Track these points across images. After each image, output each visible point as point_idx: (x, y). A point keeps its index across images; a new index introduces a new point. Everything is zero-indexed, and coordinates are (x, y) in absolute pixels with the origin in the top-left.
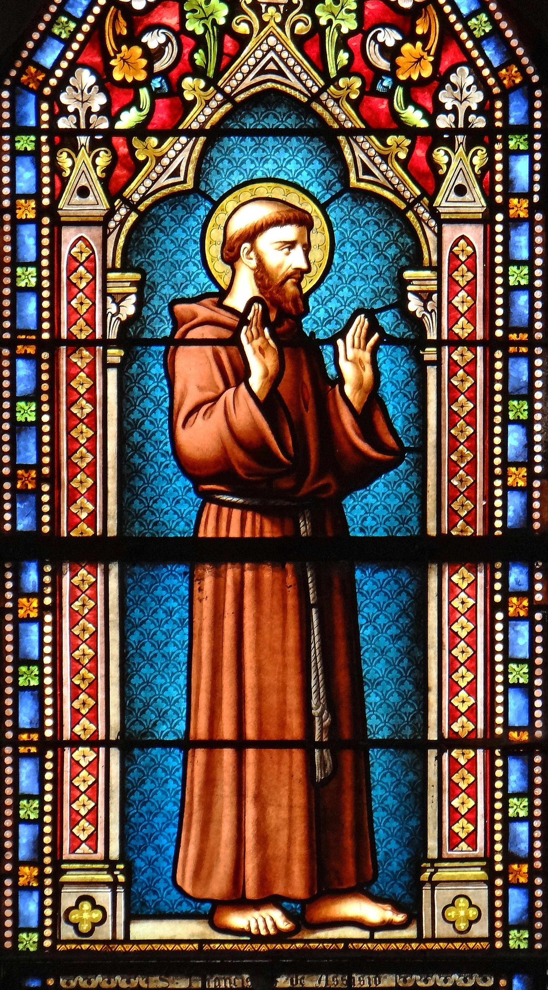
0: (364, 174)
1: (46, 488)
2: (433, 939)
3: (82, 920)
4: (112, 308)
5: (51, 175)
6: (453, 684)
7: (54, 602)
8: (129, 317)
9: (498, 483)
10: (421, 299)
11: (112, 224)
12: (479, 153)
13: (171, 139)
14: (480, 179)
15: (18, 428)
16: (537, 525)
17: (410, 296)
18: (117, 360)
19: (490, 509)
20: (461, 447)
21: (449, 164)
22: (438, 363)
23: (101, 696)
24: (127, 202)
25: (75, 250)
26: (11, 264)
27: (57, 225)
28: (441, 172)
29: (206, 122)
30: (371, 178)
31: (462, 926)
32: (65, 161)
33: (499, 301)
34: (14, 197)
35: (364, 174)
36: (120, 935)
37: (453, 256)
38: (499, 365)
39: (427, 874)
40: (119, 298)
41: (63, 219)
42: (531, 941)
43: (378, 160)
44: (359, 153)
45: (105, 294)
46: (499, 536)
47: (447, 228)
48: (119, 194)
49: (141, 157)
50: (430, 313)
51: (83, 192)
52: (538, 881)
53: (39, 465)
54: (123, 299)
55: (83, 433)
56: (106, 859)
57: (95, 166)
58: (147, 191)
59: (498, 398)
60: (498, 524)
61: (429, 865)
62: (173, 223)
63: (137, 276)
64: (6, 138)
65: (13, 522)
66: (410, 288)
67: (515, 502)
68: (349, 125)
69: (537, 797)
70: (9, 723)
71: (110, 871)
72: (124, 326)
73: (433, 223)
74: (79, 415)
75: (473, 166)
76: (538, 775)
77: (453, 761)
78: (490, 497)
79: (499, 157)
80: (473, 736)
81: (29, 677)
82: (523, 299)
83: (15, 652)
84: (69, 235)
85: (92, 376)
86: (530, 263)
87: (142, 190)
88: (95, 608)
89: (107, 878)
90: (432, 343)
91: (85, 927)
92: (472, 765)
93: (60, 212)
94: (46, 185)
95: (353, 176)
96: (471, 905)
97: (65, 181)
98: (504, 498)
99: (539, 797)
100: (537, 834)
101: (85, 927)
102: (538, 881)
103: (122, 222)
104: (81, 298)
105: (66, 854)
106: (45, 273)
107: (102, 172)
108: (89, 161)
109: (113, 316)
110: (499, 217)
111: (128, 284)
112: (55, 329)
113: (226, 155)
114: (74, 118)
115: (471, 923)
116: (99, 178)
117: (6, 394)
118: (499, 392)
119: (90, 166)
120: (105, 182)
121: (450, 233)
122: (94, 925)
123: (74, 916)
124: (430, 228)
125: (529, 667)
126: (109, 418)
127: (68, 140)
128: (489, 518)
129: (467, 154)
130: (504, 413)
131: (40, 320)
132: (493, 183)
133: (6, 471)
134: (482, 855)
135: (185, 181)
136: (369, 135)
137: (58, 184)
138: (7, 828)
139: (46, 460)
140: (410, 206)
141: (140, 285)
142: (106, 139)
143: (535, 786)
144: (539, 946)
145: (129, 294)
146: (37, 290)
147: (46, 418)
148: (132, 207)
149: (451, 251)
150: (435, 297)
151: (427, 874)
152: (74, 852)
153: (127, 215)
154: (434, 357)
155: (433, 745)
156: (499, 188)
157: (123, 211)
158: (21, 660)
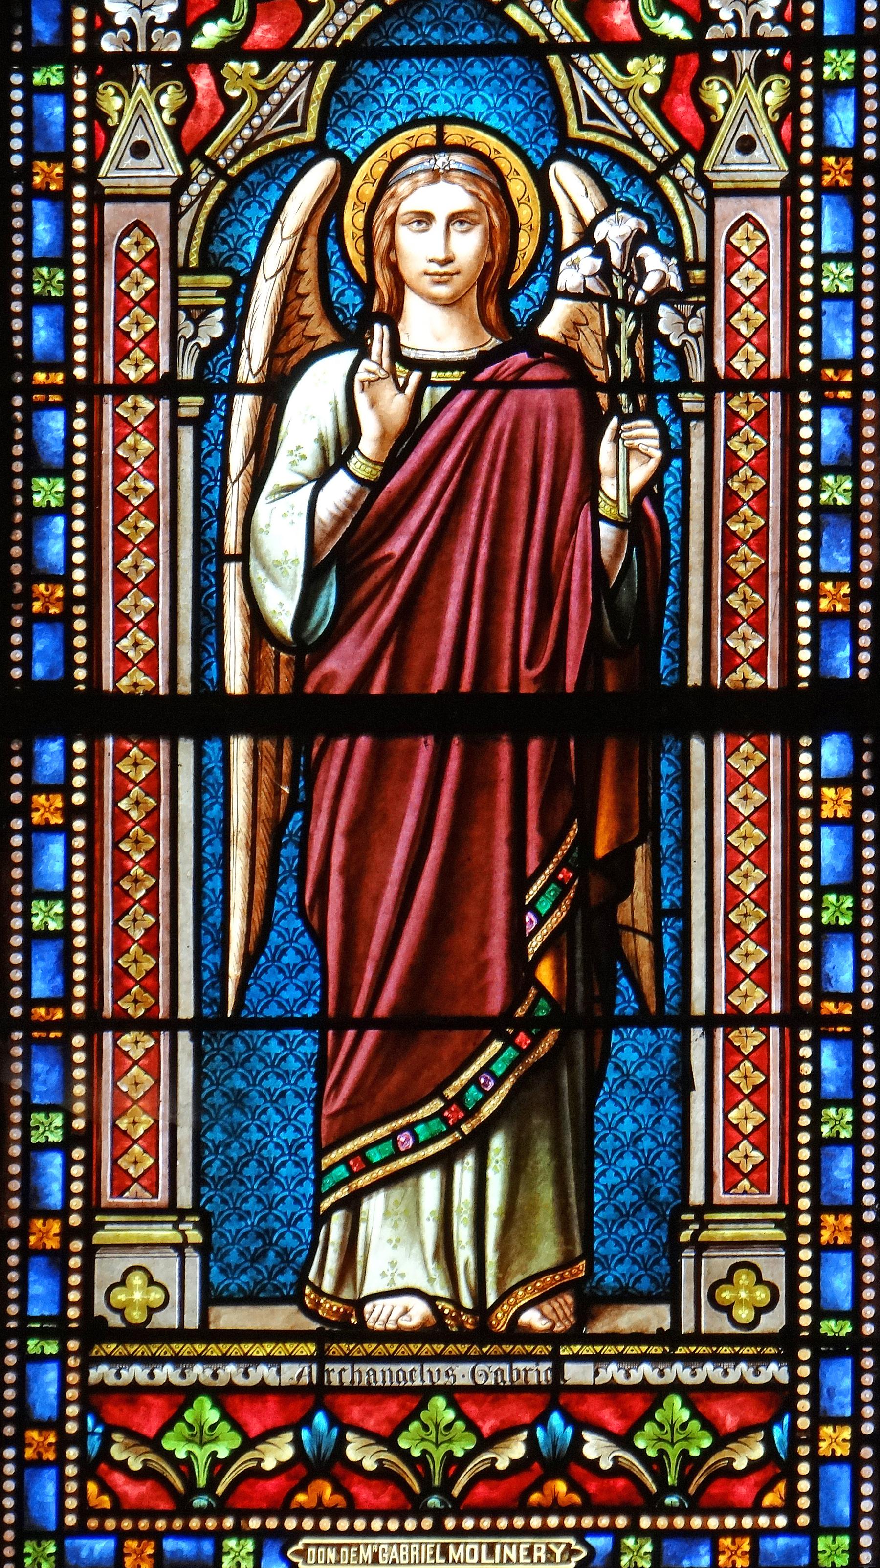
0: (590, 117)
1: (79, 825)
3: (130, 1302)
4: (187, 329)
8: (215, 20)
9: (803, 606)
11: (185, 200)
13: (281, 64)
22: (708, 417)
23: (164, 1109)
24: (209, 163)
25: (126, 241)
27: (97, 199)
29: (339, 34)
30: (602, 124)
31: (744, 1315)
32: (111, 101)
35: (590, 117)
36: (193, 1322)
38: (806, 313)
40: (196, 314)
43: (613, 96)
44: (583, 87)
45: (175, 307)
48: (198, 151)
51: (747, 145)
54: (203, 317)
56: (171, 1207)
57: (160, 109)
60: (804, 671)
61: (691, 1217)
62: (281, 976)
63: (224, 281)
65: (26, 664)
68: (565, 39)
70: (16, 993)
72: (205, 355)
73: (700, 193)
75: (765, 107)
76: (870, 80)
77: (731, 1049)
80: (763, 374)
82: (845, 1161)
83: (27, 880)
89: (173, 1236)
92: (761, 420)
93: (103, 182)
94: (78, 216)
96: (760, 1281)
97: (110, 132)
98: (815, 838)
99: (871, 1108)
102: (868, 816)
103: (204, 194)
105: (107, 1199)
107: (172, 115)
113: (368, 88)
114: (126, 34)
115: (151, 1282)
116: (166, 126)
117: (18, 255)
118: (807, 1095)
120: (174, 132)
121: (728, 210)
124: (695, 200)
126: (181, 528)
127: (119, 69)
128: (788, 662)
132: (797, 133)
135: (303, 129)
136: (596, 52)
137: (101, 135)
138: (8, 1369)
142: (179, 67)
143: (863, 878)
145: (213, 308)
147: (79, 925)
153: (211, 185)
154: (701, 408)
157: (204, 178)
158: (36, 466)
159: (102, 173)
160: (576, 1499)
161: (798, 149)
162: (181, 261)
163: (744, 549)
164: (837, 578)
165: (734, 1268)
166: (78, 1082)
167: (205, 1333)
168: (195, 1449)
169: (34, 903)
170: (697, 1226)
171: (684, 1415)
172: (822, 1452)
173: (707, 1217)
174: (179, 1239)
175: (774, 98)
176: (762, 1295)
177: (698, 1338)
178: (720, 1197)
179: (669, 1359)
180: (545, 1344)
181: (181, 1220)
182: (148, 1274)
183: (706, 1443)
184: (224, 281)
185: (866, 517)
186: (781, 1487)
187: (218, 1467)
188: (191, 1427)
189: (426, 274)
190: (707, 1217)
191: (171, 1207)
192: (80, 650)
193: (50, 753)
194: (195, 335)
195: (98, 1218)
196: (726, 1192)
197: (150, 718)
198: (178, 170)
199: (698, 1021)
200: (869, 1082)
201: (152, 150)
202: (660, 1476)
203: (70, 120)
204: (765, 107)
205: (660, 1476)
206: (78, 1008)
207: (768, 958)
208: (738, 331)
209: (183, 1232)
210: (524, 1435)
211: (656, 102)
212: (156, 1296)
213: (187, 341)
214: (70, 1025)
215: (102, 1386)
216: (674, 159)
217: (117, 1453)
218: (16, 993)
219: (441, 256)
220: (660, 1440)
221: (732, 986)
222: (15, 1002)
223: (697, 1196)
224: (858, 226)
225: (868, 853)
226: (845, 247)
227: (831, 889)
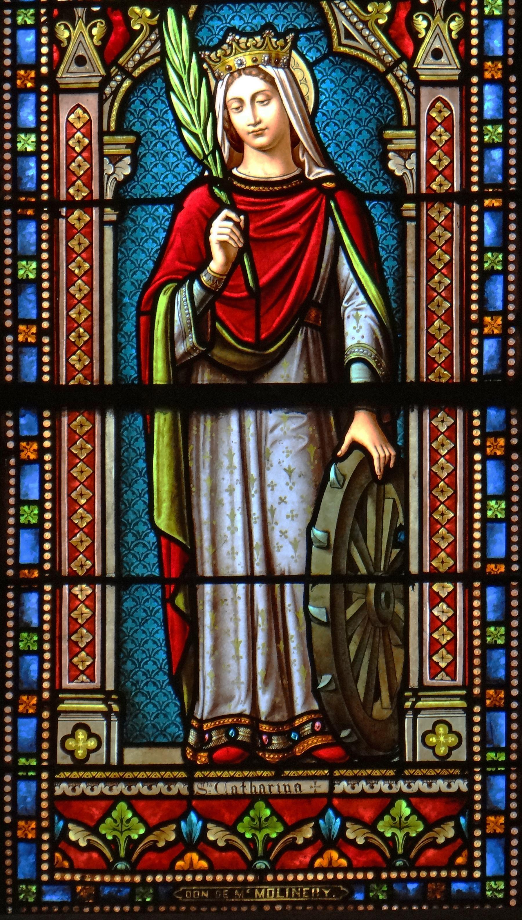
0: (346, 38)
4: (109, 169)
5: (49, 45)
7: (53, 566)
11: (108, 91)
12: (457, 19)
14: (455, 43)
15: (20, 285)
18: (114, 218)
20: (442, 483)
22: (417, 219)
31: (442, 751)
33: (477, 535)
34: (15, 67)
35: (346, 38)
36: (114, 760)
37: (430, 119)
41: (61, 86)
46: (475, 383)
47: (424, 91)
48: (115, 62)
49: (137, 27)
51: (81, 61)
52: (515, 831)
53: (39, 320)
56: (102, 689)
57: (92, 36)
63: (131, 139)
64: (8, 12)
66: (390, 147)
67: (490, 347)
70: (10, 562)
71: (104, 701)
72: (119, 185)
73: (411, 85)
81: (29, 514)
82: (497, 154)
84: (66, 103)
88: (93, 522)
89: (101, 707)
90: (410, 199)
91: (80, 753)
97: (63, 51)
100: (512, 287)
101: (80, 753)
102: (515, 831)
104: (78, 196)
105: (66, 684)
107: (458, 34)
110: (475, 80)
111: (124, 146)
112: (53, 191)
115: (451, 731)
116: (95, 46)
119: (86, 34)
120: (100, 50)
122: (90, 752)
123: (70, 744)
125: (503, 128)
128: (466, 365)
131: (40, 182)
133: (8, 73)
137: (56, 55)
139: (45, 315)
140: (390, 69)
141: (134, 147)
145: (125, 156)
148: (127, 74)
154: (413, 213)
156: (474, 52)
159: (59, 75)
160: (344, 862)
162: (105, 128)
165: (435, 724)
167: (121, 766)
168: (397, 832)
169: (21, 508)
171: (407, 811)
173: (420, 694)
176: (452, 740)
177: (415, 765)
179: (396, 778)
180: (456, 768)
182: (87, 731)
183: (142, 831)
184: (131, 139)
186: (465, 853)
187: (410, 842)
188: (115, 821)
189: (249, 133)
190: (420, 694)
191: (102, 689)
193: (26, 421)
197: (90, 399)
198: (103, 72)
199: (260, 579)
201: (444, 54)
202: (115, 852)
203: (38, 45)
205: (115, 852)
210: (312, 824)
211: (385, 29)
212: (92, 743)
213: (109, 176)
215: (64, 796)
216: (397, 63)
217: (350, 835)
218: (10, 562)
219: (252, 122)
220: (114, 829)
222: (9, 567)
223: (414, 682)
225: (513, 100)
227: (492, 497)
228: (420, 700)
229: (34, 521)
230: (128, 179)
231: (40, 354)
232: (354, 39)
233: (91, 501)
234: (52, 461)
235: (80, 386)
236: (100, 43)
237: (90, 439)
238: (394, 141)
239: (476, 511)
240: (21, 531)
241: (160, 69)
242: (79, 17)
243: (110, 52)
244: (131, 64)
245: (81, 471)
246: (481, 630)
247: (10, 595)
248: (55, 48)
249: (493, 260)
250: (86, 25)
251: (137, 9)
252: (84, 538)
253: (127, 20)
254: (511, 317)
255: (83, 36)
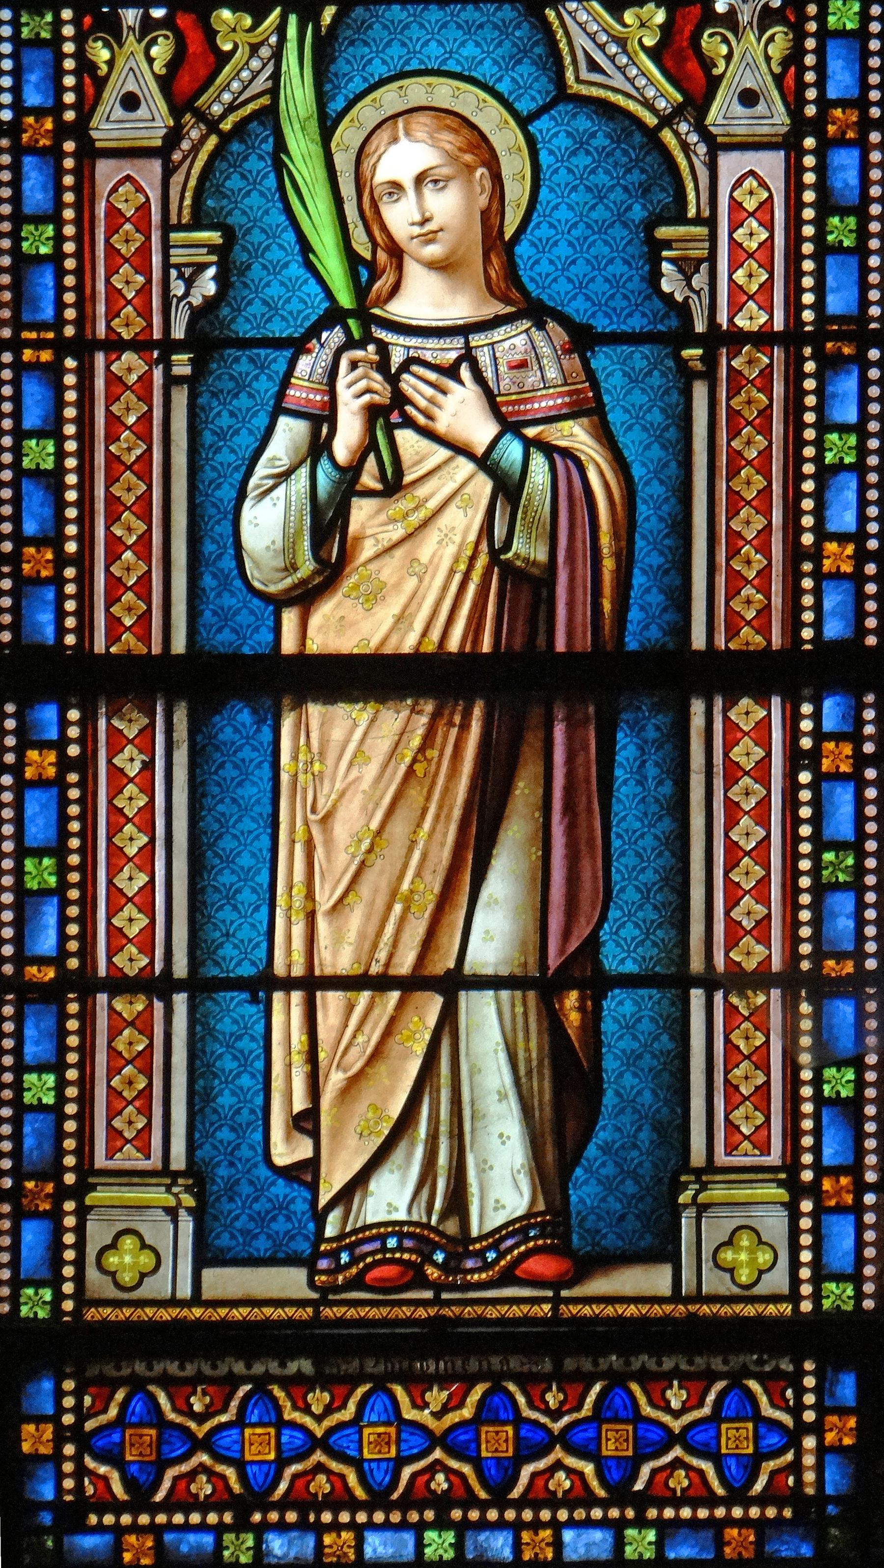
2: (699, 1298)
4: (178, 288)
6: (732, 847)
7: (83, 964)
10: (681, 270)
11: (177, 156)
14: (779, 80)
16: (871, 641)
17: (666, 267)
18: (187, 370)
19: (794, 609)
21: (729, 58)
22: (710, 375)
24: (201, 116)
26: (13, 1069)
27: (89, 153)
28: (716, 72)
31: (744, 1276)
36: (185, 1291)
37: (736, 205)
39: (690, 1193)
40: (188, 272)
41: (98, 144)
42: (859, 1296)
45: (166, 266)
49: (228, 47)
50: (698, 293)
55: (133, 841)
56: (165, 1171)
57: (150, 60)
58: (235, 99)
59: (805, 848)
60: (807, 633)
61: (693, 1178)
63: (214, 237)
69: (870, 888)
72: (197, 315)
74: (123, 251)
75: (768, 59)
78: (794, 593)
79: (810, 44)
84: (107, 172)
85: (146, 397)
86: (860, 429)
87: (227, 97)
95: (570, 75)
97: (101, 83)
102: (871, 774)
105: (100, 1161)
106: (71, 446)
108: (139, 48)
109: (180, 299)
117: (8, 1060)
119: (141, 57)
120: (165, 83)
121: (731, 165)
126: (173, 1129)
128: (793, 624)
129: (759, 40)
130: (819, 238)
132: (802, 86)
134: (778, 1162)
137: (90, 90)
141: (223, 252)
144: (871, 641)
146: (57, 1110)
148: (213, 125)
149: (731, 197)
150: (704, 267)
151: (690, 1193)
152: (111, 1158)
153: (203, 140)
155: (697, 982)
157: (195, 134)
161: (802, 102)
162: (174, 220)
163: (746, 781)
164: (842, 538)
166: (70, 538)
170: (697, 1186)
172: (826, 569)
174: (172, 1202)
175: (777, 51)
178: (721, 1158)
181: (174, 1183)
185: (870, 1110)
191: (165, 1171)
192: (72, 1033)
194: (187, 294)
195: (91, 1180)
196: (728, 1154)
200: (871, 623)
204: (768, 59)
206: (69, 331)
207: (771, 365)
208: (738, 1048)
209: (176, 1195)
214: (61, 347)
221: (732, 942)
224: (864, 287)
225: (871, 606)
226: (848, 1159)
228: (706, 1189)
229: (49, 1099)
230: (211, 304)
231: (61, 597)
232: (602, 71)
233: (146, 418)
234: (80, 785)
235: (128, 657)
236: (164, 71)
237: (144, 473)
238: (674, 245)
239: (805, 1133)
240: (28, 954)
241: (270, 115)
242: (129, 27)
243: (182, 88)
244: (217, 109)
245: (129, 530)
246: (812, 962)
247: (8, 1010)
248: (87, 80)
249: (840, 448)
250: (139, 41)
251: (226, 14)
252: (136, 914)
253: (211, 34)
254: (873, 544)
255: (137, 64)
